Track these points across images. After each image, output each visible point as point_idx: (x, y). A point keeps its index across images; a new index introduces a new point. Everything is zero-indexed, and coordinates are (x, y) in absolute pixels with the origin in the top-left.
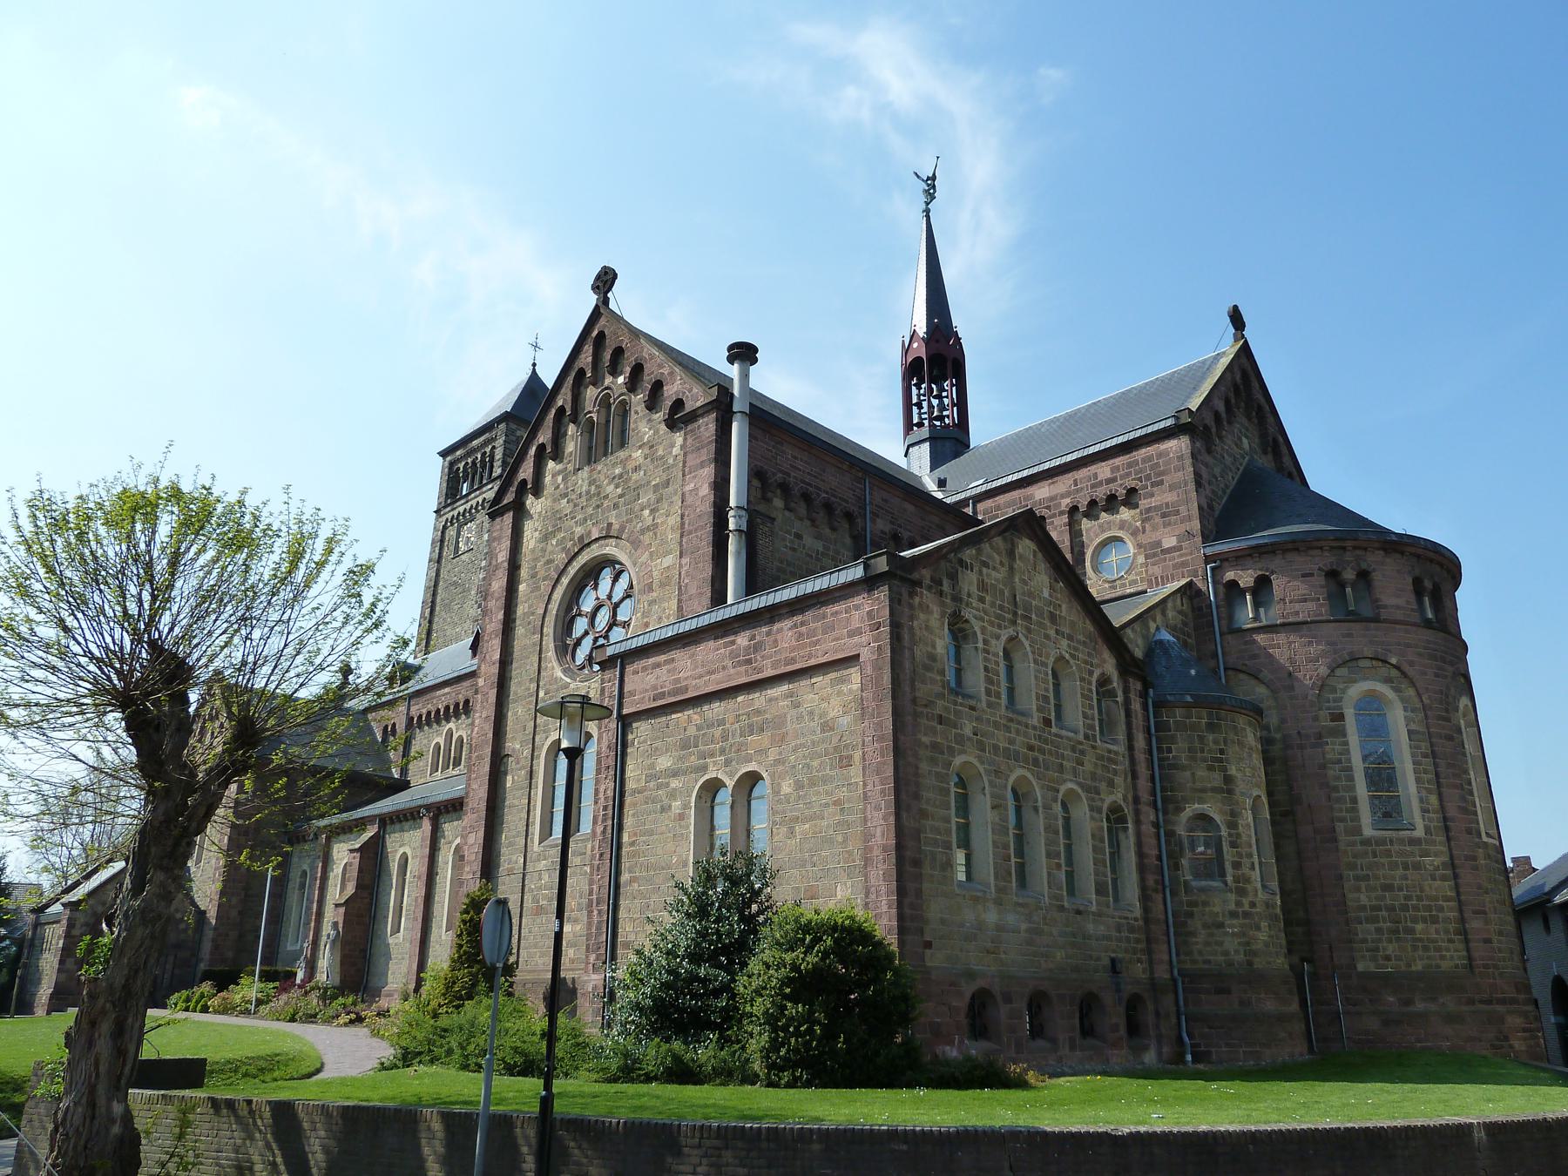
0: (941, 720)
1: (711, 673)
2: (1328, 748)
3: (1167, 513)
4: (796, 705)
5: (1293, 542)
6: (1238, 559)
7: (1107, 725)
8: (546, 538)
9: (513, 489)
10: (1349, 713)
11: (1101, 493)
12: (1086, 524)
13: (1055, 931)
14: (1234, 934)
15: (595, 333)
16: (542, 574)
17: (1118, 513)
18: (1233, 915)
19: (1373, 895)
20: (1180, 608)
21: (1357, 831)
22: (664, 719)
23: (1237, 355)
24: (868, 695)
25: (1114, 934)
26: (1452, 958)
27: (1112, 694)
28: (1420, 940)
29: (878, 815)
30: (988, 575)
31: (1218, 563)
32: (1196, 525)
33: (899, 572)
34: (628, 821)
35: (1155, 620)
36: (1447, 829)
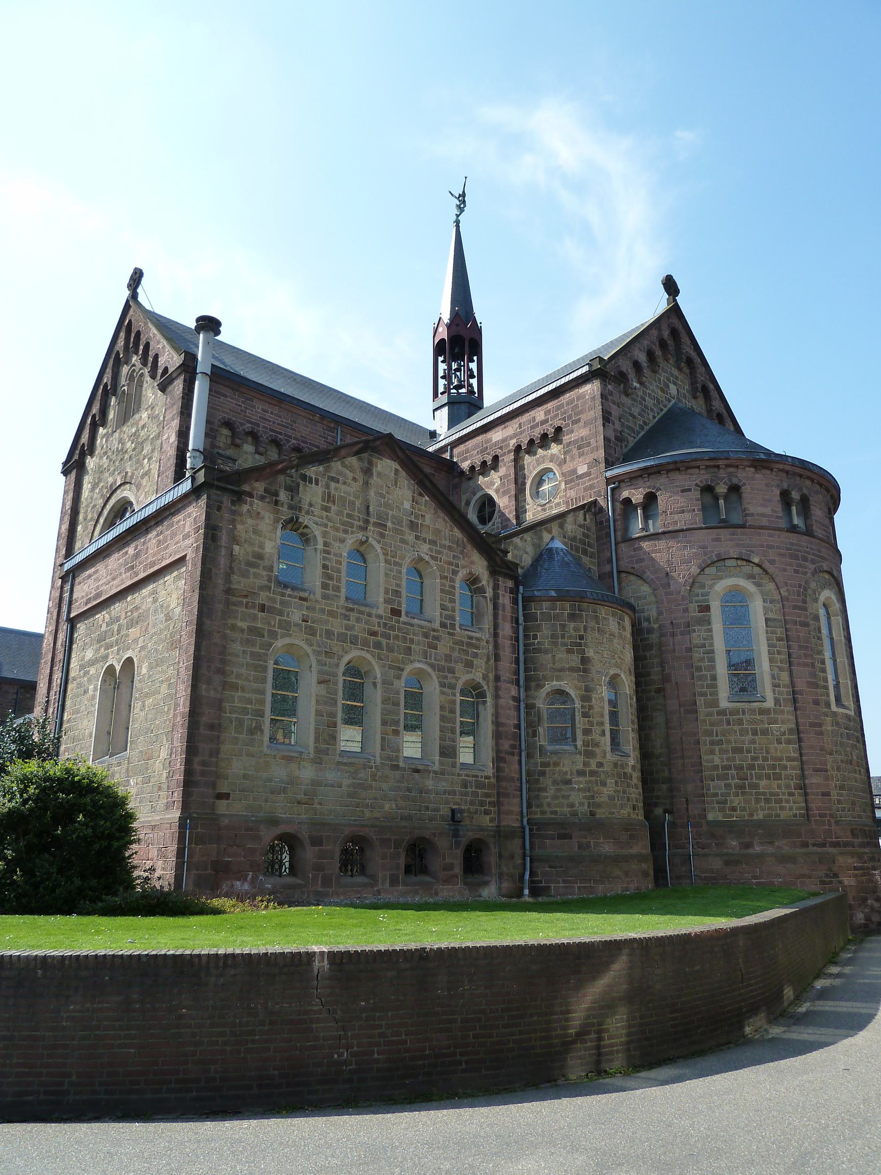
0: (262, 608)
2: (694, 635)
3: (581, 445)
5: (675, 462)
6: (631, 479)
7: (476, 617)
8: (93, 490)
10: (715, 606)
11: (537, 433)
12: (527, 459)
13: (384, 786)
14: (579, 790)
17: (549, 448)
18: (581, 773)
19: (725, 756)
20: (582, 522)
21: (715, 703)
22: (92, 619)
25: (458, 789)
26: (791, 809)
27: (481, 591)
28: (764, 794)
32: (601, 454)
33: (216, 483)
34: (68, 703)
35: (550, 532)
36: (795, 701)
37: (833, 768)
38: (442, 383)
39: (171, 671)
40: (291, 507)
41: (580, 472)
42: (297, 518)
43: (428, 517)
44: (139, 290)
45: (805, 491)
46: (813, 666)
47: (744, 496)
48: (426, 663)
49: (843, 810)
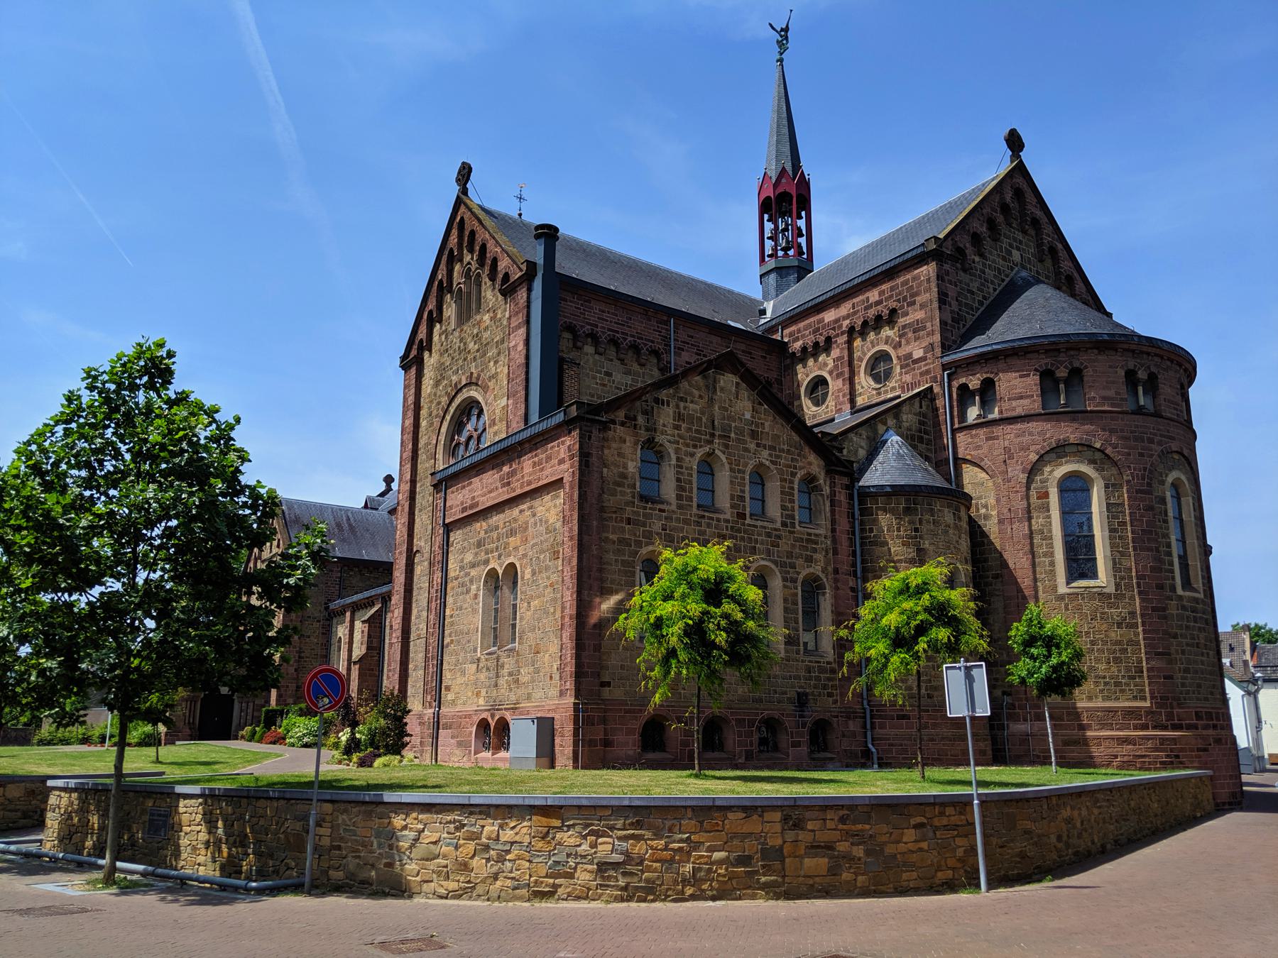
0: (629, 521)
1: (490, 492)
4: (534, 515)
8: (437, 384)
9: (415, 347)
11: (872, 313)
15: (458, 218)
16: (435, 413)
21: (1055, 588)
23: (1010, 175)
24: (567, 507)
27: (818, 489)
29: (569, 593)
30: (685, 408)
31: (953, 369)
34: (450, 600)
35: (885, 423)
37: (1177, 651)
38: (769, 244)
39: (554, 578)
40: (647, 430)
41: (916, 356)
42: (654, 438)
43: (767, 424)
44: (468, 186)
45: (1153, 369)
46: (1158, 551)
47: (1085, 379)
48: (770, 560)
49: (1188, 692)
